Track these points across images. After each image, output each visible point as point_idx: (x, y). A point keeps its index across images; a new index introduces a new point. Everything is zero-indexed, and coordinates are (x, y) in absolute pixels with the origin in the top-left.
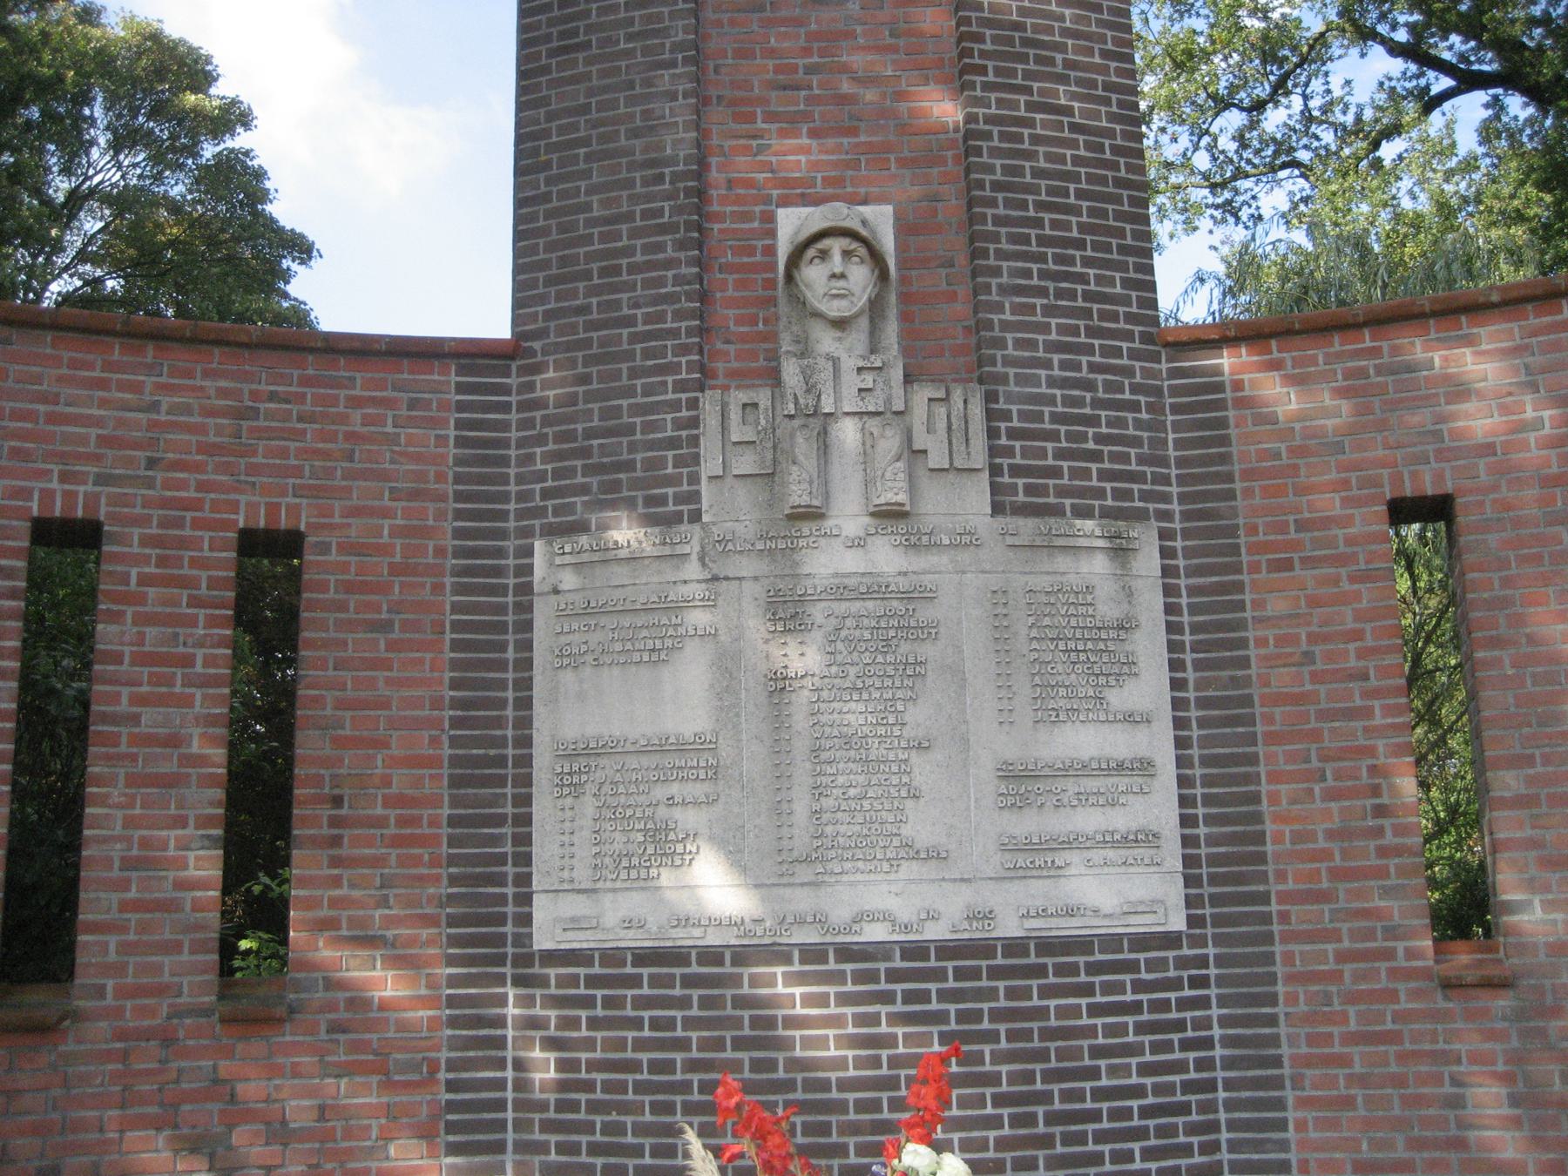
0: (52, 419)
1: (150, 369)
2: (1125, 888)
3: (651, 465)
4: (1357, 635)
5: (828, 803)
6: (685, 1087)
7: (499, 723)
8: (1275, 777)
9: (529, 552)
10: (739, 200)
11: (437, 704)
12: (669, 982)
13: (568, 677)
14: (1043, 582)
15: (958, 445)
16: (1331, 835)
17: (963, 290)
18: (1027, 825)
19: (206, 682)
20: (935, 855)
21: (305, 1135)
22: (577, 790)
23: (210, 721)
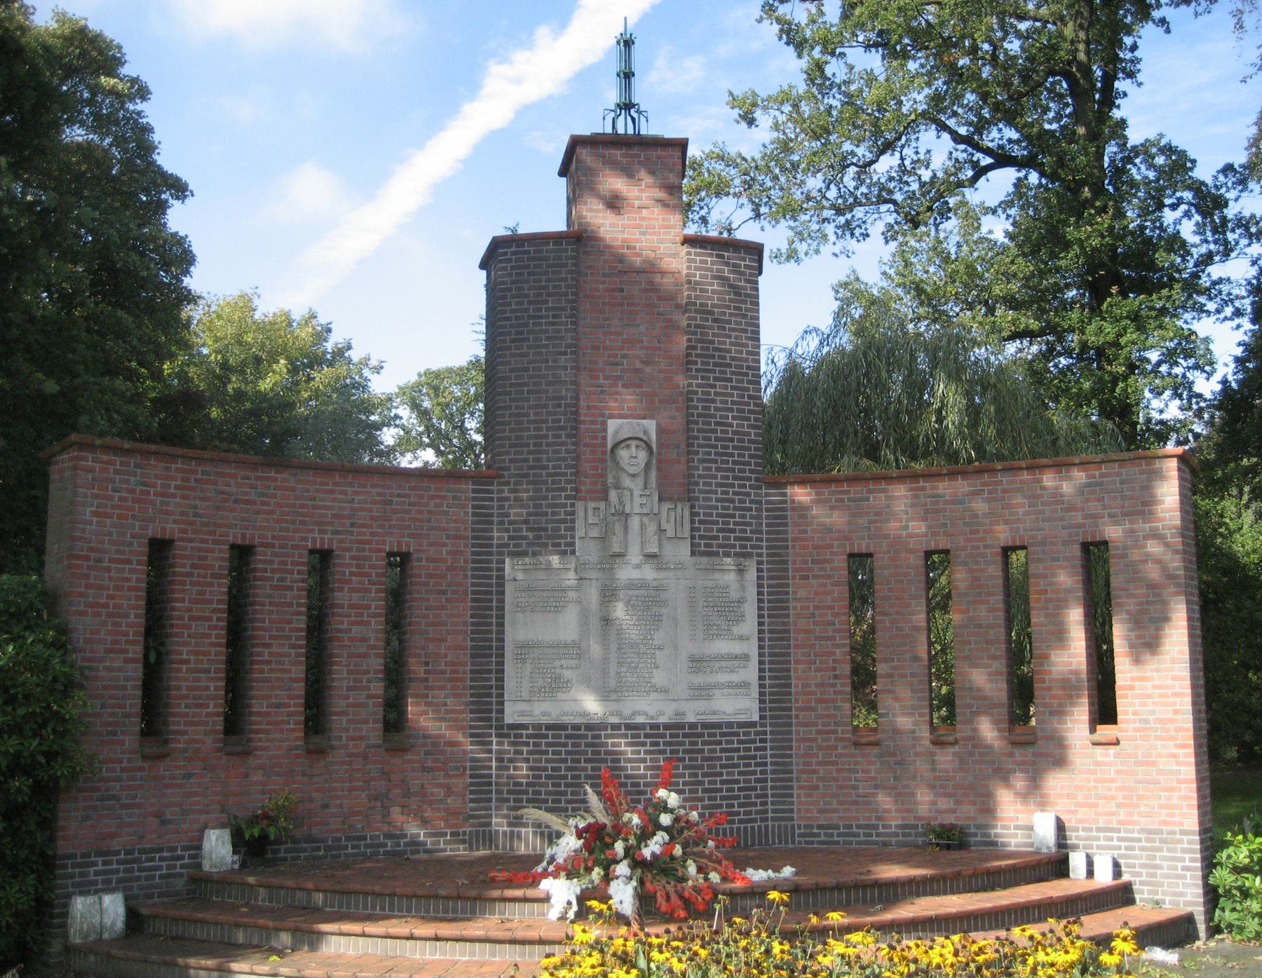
0: (315, 507)
1: (351, 484)
2: (737, 705)
3: (554, 529)
4: (832, 607)
5: (624, 669)
6: (565, 777)
7: (490, 632)
8: (797, 662)
9: (504, 562)
10: (592, 415)
11: (465, 624)
12: (560, 736)
13: (519, 615)
14: (709, 584)
15: (679, 528)
16: (817, 685)
17: (683, 459)
18: (699, 679)
19: (376, 615)
20: (664, 691)
21: (416, 794)
22: (524, 661)
23: (378, 631)
